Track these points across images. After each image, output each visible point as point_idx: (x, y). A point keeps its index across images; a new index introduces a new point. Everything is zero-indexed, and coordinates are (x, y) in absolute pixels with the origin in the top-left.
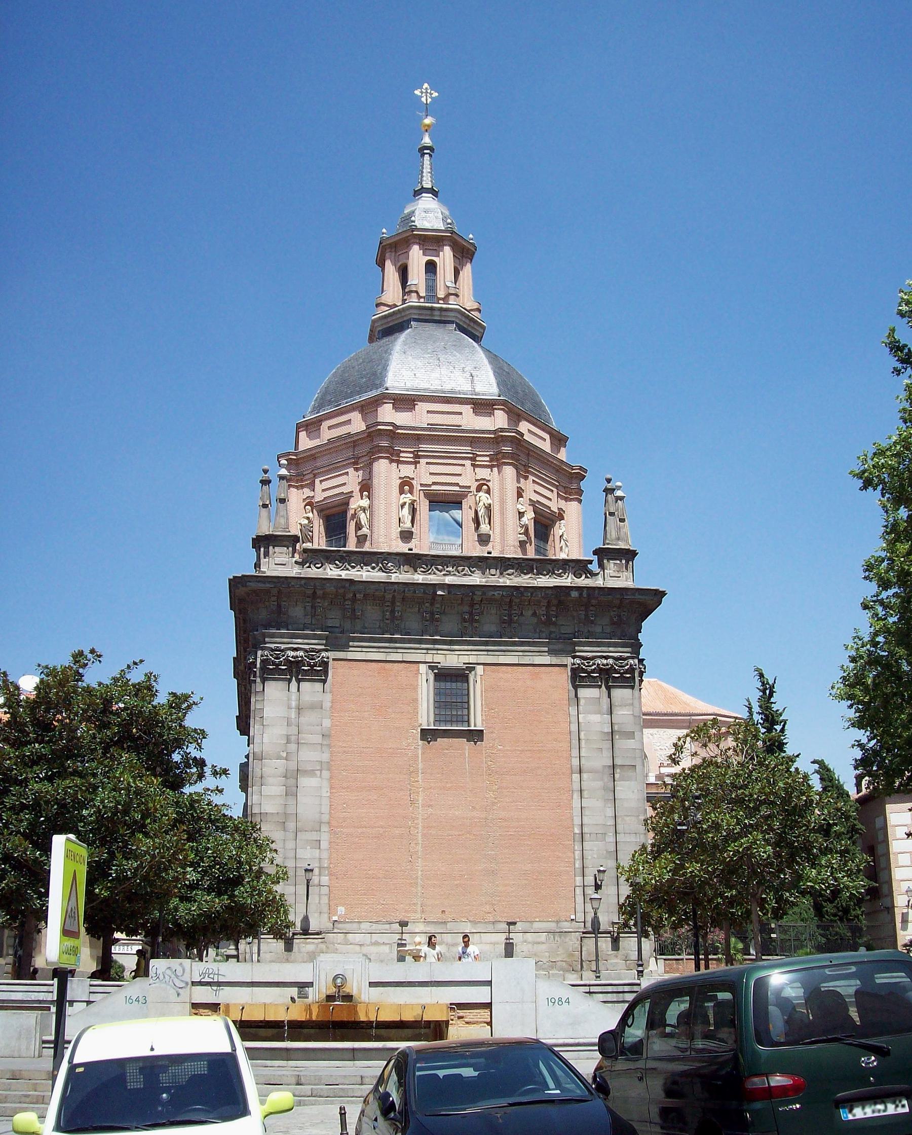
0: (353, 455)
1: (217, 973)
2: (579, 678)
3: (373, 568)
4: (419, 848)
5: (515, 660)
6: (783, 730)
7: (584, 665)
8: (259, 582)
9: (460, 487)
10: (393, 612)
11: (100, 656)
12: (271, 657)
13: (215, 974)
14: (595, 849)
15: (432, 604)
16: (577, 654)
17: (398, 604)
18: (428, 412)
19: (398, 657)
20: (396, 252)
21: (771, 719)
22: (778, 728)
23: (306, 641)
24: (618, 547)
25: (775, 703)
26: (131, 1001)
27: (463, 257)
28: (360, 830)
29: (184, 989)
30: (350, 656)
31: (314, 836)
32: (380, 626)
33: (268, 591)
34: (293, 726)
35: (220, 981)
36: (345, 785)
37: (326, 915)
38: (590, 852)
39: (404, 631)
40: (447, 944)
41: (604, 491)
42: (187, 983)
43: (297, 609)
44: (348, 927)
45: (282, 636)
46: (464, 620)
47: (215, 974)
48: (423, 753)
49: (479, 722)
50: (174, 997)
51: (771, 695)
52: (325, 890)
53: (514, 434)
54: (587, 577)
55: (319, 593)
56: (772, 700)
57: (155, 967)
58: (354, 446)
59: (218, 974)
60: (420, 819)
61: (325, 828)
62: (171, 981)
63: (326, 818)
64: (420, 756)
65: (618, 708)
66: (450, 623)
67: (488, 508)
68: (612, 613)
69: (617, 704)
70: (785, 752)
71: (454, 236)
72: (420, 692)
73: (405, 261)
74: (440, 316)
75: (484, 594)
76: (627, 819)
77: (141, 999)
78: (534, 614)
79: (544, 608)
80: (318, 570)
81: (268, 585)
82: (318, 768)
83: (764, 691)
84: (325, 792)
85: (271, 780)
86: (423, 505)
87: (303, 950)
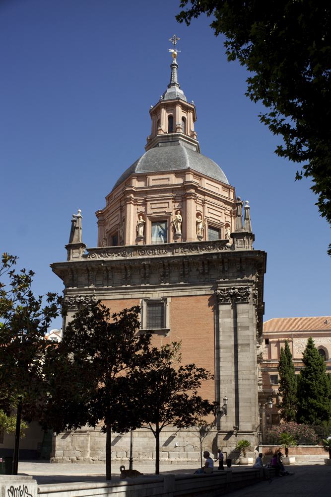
2: (216, 301)
3: (119, 255)
5: (187, 294)
8: (61, 266)
9: (167, 213)
10: (127, 275)
16: (219, 288)
18: (153, 180)
19: (129, 296)
20: (156, 115)
23: (85, 292)
38: (224, 390)
40: (148, 437)
43: (82, 277)
45: (75, 290)
54: (226, 249)
55: (90, 268)
58: (121, 202)
66: (154, 278)
75: (168, 261)
78: (197, 270)
79: (201, 266)
81: (65, 267)
86: (149, 223)
87: (79, 440)
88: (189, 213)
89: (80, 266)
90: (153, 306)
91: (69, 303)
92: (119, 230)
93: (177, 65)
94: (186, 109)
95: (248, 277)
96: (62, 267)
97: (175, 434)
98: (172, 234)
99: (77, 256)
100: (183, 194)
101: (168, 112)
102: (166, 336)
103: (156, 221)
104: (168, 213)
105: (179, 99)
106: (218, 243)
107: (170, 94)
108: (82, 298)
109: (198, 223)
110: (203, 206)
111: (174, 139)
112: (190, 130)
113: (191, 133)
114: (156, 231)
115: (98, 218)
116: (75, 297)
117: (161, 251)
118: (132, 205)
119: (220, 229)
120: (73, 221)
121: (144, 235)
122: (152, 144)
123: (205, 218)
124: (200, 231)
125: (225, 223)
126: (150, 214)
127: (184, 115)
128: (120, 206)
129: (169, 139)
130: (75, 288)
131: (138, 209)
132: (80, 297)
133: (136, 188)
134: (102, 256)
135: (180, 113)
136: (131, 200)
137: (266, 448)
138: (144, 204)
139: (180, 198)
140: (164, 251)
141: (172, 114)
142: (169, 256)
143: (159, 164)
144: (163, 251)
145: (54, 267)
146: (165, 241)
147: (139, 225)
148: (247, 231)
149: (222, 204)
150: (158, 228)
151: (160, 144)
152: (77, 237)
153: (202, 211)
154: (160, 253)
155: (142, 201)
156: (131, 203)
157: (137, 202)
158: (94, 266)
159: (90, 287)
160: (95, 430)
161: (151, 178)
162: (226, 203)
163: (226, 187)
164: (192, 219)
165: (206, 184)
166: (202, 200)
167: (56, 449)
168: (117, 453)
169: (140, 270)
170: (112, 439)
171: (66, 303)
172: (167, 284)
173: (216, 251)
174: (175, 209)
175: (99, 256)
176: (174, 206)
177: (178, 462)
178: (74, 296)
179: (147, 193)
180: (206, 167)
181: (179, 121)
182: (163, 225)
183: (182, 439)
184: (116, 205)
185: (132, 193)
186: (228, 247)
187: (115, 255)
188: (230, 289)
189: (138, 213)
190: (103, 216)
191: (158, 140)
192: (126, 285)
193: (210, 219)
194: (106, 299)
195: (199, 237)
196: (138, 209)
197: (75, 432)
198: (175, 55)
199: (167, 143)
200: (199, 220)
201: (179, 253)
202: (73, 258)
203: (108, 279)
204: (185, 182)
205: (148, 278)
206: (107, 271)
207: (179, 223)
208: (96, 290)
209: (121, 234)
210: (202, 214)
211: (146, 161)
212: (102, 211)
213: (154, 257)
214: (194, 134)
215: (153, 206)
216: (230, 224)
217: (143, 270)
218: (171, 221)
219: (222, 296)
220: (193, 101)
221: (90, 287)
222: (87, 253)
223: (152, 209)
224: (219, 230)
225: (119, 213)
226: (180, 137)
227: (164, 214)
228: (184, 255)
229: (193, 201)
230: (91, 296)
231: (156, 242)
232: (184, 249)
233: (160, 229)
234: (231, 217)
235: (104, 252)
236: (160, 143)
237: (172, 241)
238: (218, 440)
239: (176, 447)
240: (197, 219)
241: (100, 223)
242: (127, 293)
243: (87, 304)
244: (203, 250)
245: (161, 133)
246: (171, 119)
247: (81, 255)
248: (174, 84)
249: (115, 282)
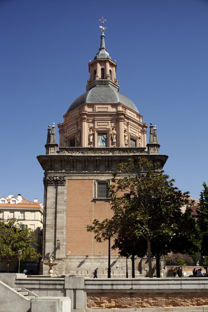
3: (80, 153)
8: (45, 157)
9: (107, 129)
10: (85, 165)
15: (97, 162)
17: (86, 162)
18: (98, 108)
19: (87, 178)
23: (59, 174)
28: (75, 229)
30: (73, 178)
31: (61, 231)
36: (71, 216)
37: (65, 254)
43: (57, 165)
44: (71, 257)
46: (106, 167)
52: (65, 247)
54: (144, 153)
55: (63, 160)
58: (77, 119)
61: (64, 228)
63: (65, 225)
66: (102, 168)
73: (95, 69)
74: (105, 83)
75: (112, 158)
81: (47, 158)
82: (63, 211)
84: (65, 218)
85: (49, 215)
86: (96, 134)
88: (121, 130)
89: (57, 158)
90: (101, 185)
91: (49, 181)
92: (76, 137)
93: (104, 37)
94: (112, 65)
95: (157, 170)
96: (45, 158)
97: (117, 260)
98: (110, 142)
99: (53, 152)
100: (117, 118)
101: (101, 65)
102: (96, 203)
103: (100, 133)
104: (108, 129)
105: (109, 59)
106: (139, 149)
107: (102, 54)
108: (58, 178)
109: (125, 136)
110: (127, 126)
111: (106, 83)
112: (114, 78)
113: (115, 80)
114: (100, 139)
115: (59, 128)
116: (53, 177)
117: (106, 152)
118: (86, 122)
119: (136, 140)
120: (49, 130)
121: (93, 141)
122: (92, 85)
123: (129, 133)
124: (126, 141)
125: (138, 136)
126: (97, 129)
127: (111, 68)
128: (77, 122)
129: (103, 83)
130: (52, 171)
131: (89, 125)
132: (56, 177)
133: (88, 112)
134: (69, 152)
135: (108, 67)
136: (85, 119)
137: (169, 268)
138: (93, 122)
139: (114, 120)
140: (108, 152)
141: (104, 67)
142: (111, 155)
143: (101, 98)
144: (107, 152)
145: (39, 158)
146: (106, 146)
147: (90, 135)
148: (156, 143)
149: (137, 125)
150: (102, 138)
151: (97, 85)
152: (53, 140)
153: (127, 129)
154: (105, 153)
155: (91, 120)
156: (85, 121)
157: (88, 120)
158: (66, 158)
159: (63, 171)
160: (68, 258)
161: (97, 106)
162: (139, 125)
163: (139, 116)
164: (122, 134)
165: (128, 113)
166: (127, 123)
167: (43, 270)
168: (81, 272)
169: (93, 162)
170: (111, 263)
171: (47, 180)
172: (86, 172)
173: (139, 154)
174: (112, 127)
175: (67, 152)
176: (111, 125)
177: (119, 276)
178: (52, 176)
179: (94, 115)
180: (127, 102)
181: (108, 73)
182: (105, 136)
183: (121, 263)
184: (73, 121)
185: (86, 115)
186: (145, 152)
187: (77, 153)
188: (54, 177)
189: (89, 127)
190: (63, 127)
191: (96, 83)
192: (85, 171)
193: (131, 134)
194: (72, 179)
195: (126, 145)
196: (89, 125)
197: (55, 259)
198: (103, 30)
199: (102, 85)
200: (126, 135)
201: (117, 154)
202: (51, 152)
203: (73, 167)
204: (118, 111)
205: (98, 168)
206: (73, 162)
207: (115, 136)
208: (66, 173)
209: (78, 139)
210: (127, 130)
211: (92, 96)
212: (62, 124)
213: (101, 155)
214: (117, 81)
215: (99, 124)
216: (141, 138)
217: (95, 162)
218: (110, 134)
219: (60, 181)
220: (115, 61)
221: (63, 171)
222: (58, 150)
223: (98, 125)
224: (135, 141)
225: (76, 126)
226: (110, 82)
227: (105, 129)
228: (120, 155)
229: (123, 123)
230: (63, 177)
231: (101, 146)
232: (119, 151)
233: (103, 138)
234: (141, 133)
235: (70, 150)
236: (97, 84)
237: (111, 146)
238: (142, 264)
239: (117, 267)
240: (124, 134)
241: (61, 131)
242: (86, 176)
243: (61, 181)
244: (131, 153)
245: (97, 79)
246: (103, 70)
247: (56, 151)
248: (103, 48)
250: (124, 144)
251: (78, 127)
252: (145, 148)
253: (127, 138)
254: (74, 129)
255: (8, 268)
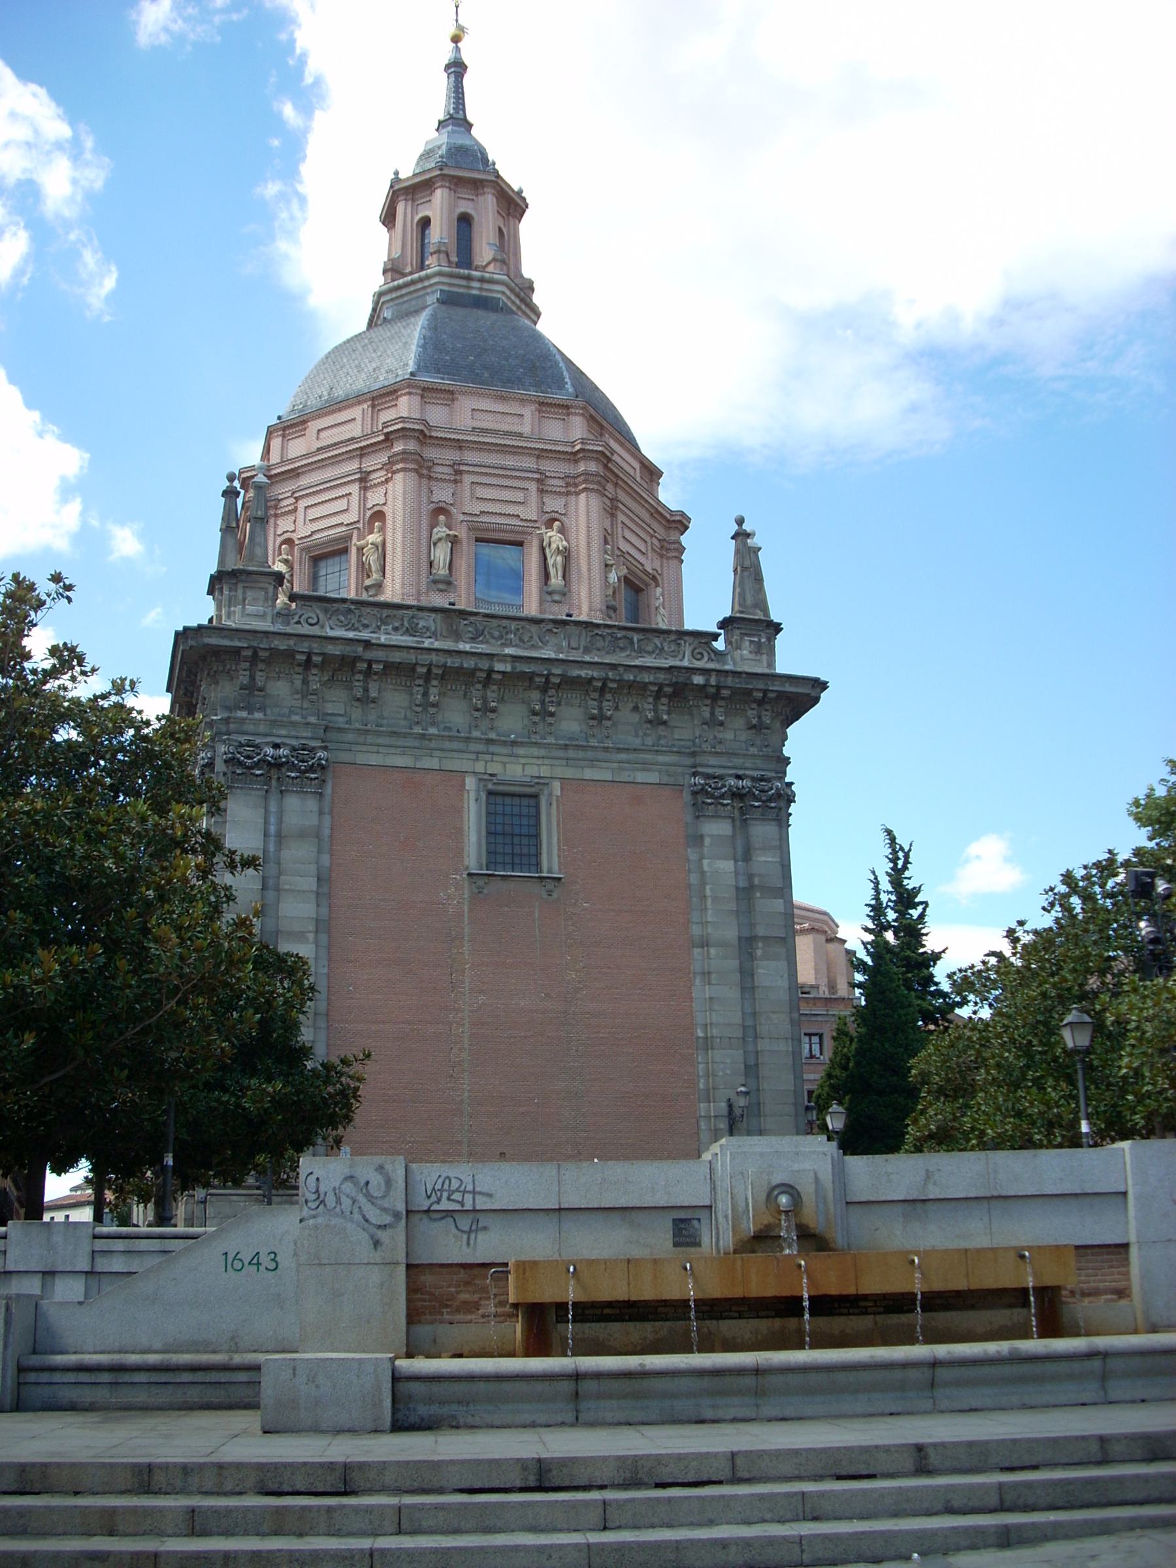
0: (360, 468)
1: (470, 1188)
4: (464, 1055)
6: (922, 916)
7: (710, 787)
11: (69, 588)
12: (239, 756)
13: (465, 1192)
14: (728, 1061)
21: (906, 898)
22: (915, 913)
24: (757, 617)
25: (909, 878)
26: (238, 1265)
27: (508, 214)
29: (389, 1232)
32: (405, 715)
33: (237, 651)
34: (272, 864)
35: (478, 1208)
38: (722, 1066)
39: (442, 726)
41: (733, 538)
42: (397, 1215)
47: (465, 1192)
48: (470, 911)
49: (556, 867)
50: (364, 1251)
51: (905, 868)
53: (600, 449)
56: (907, 874)
57: (312, 1178)
59: (474, 1192)
60: (466, 1012)
62: (356, 1210)
64: (466, 915)
65: (758, 852)
67: (566, 554)
68: (750, 712)
69: (757, 846)
70: (924, 946)
71: (499, 181)
72: (466, 819)
76: (774, 1016)
77: (265, 1260)
80: (313, 628)
83: (894, 860)
128: (360, 471)
132: (276, 746)
193: (627, 556)
215: (481, 492)
219: (293, 767)
225: (354, 489)
227: (344, 529)
249: (385, 714)
250: (585, 608)
251: (369, 494)
252: (715, 637)
253: (613, 577)
254: (341, 505)
255: (922, 950)
